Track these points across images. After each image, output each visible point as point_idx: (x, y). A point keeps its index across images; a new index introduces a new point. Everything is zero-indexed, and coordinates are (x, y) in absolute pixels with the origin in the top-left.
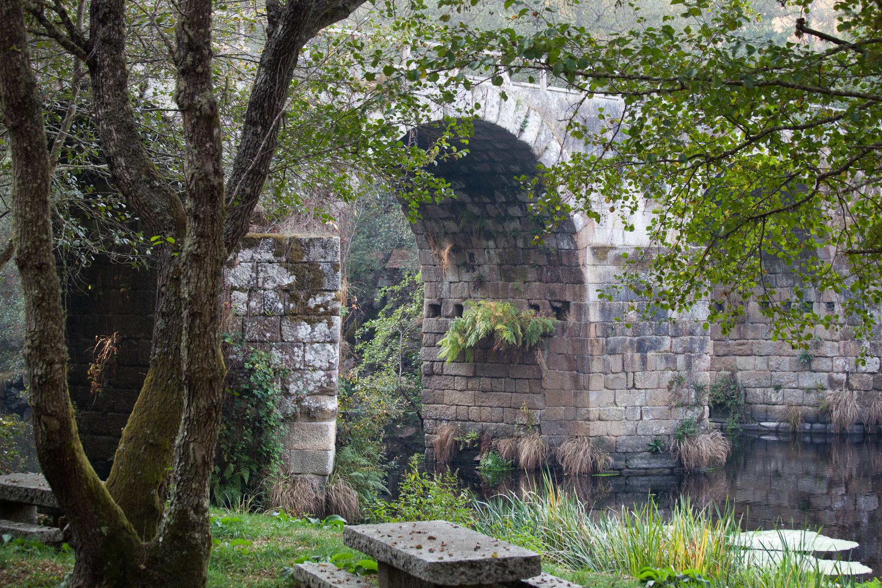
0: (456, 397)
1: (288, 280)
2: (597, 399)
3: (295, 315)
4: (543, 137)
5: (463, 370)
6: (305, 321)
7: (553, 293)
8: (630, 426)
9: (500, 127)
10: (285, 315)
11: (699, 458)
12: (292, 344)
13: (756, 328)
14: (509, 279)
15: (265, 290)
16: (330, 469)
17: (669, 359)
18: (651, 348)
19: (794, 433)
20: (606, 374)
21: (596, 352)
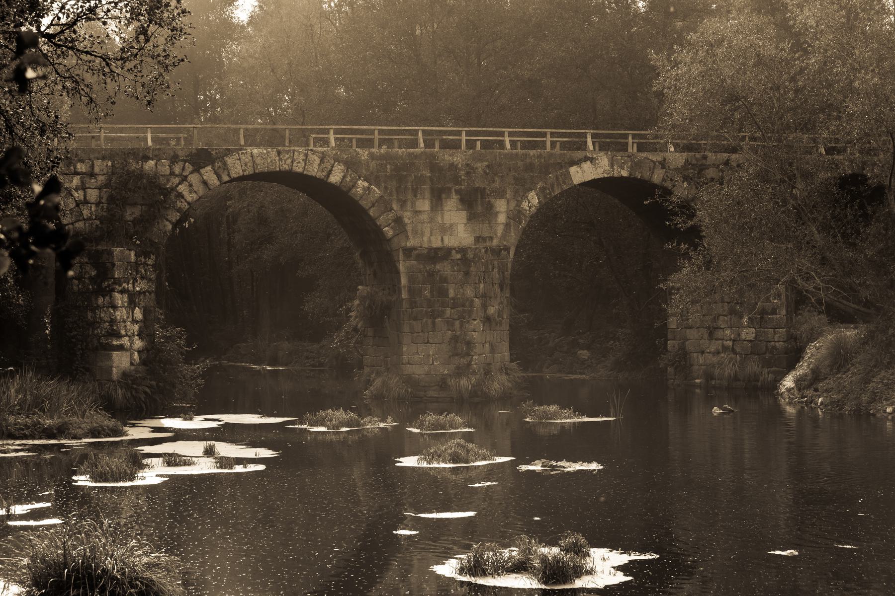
4: (348, 179)
8: (426, 368)
9: (307, 176)
17: (450, 323)
18: (438, 316)
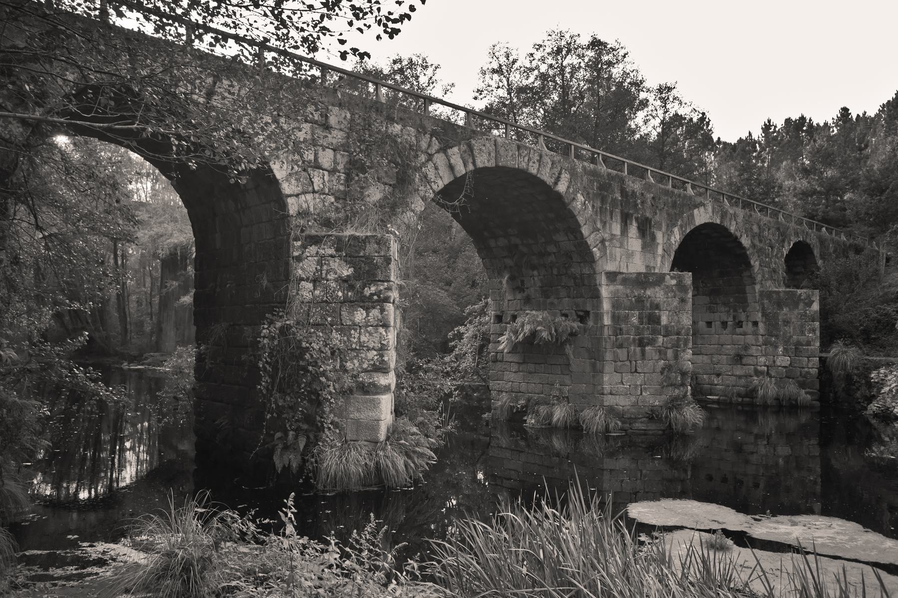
0: (512, 376)
1: (347, 272)
2: (609, 380)
3: (351, 302)
4: (571, 190)
5: (515, 358)
6: (361, 307)
7: (577, 305)
8: (633, 399)
9: (539, 178)
10: (345, 302)
11: (685, 425)
12: (350, 328)
13: (704, 338)
14: (548, 297)
15: (327, 280)
16: (382, 436)
17: (662, 353)
18: (648, 344)
19: (731, 403)
20: (615, 362)
21: (609, 346)
